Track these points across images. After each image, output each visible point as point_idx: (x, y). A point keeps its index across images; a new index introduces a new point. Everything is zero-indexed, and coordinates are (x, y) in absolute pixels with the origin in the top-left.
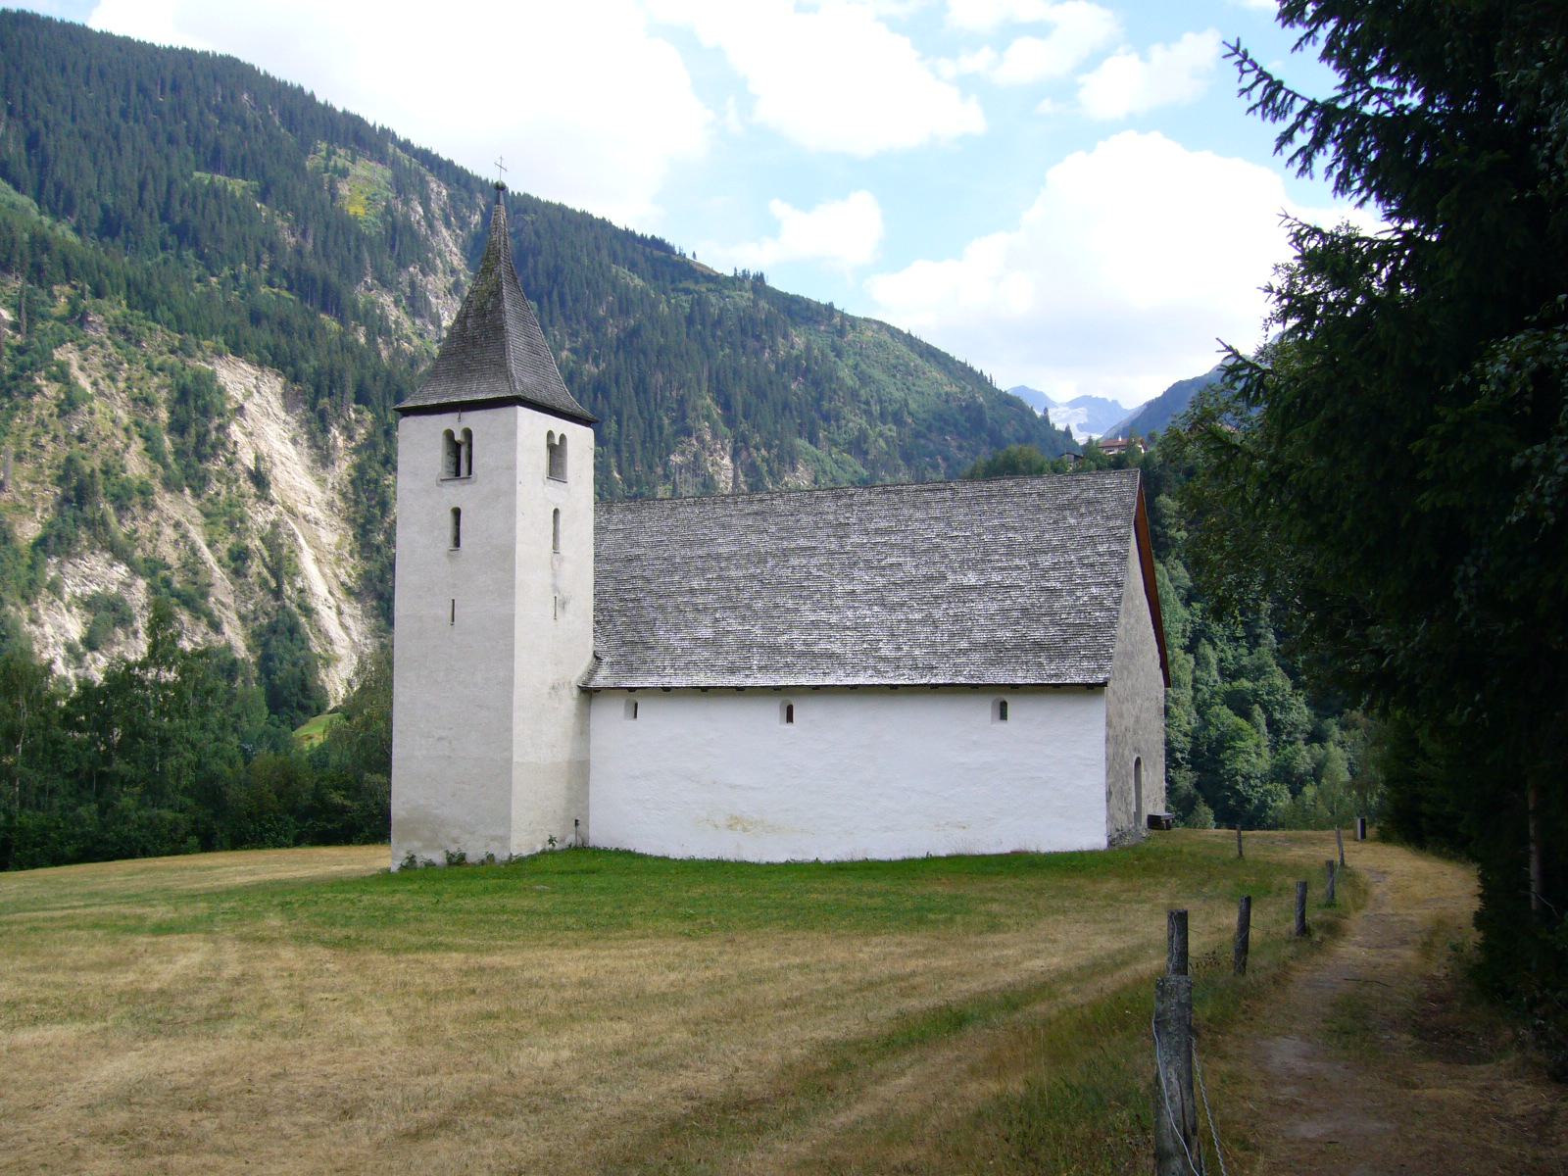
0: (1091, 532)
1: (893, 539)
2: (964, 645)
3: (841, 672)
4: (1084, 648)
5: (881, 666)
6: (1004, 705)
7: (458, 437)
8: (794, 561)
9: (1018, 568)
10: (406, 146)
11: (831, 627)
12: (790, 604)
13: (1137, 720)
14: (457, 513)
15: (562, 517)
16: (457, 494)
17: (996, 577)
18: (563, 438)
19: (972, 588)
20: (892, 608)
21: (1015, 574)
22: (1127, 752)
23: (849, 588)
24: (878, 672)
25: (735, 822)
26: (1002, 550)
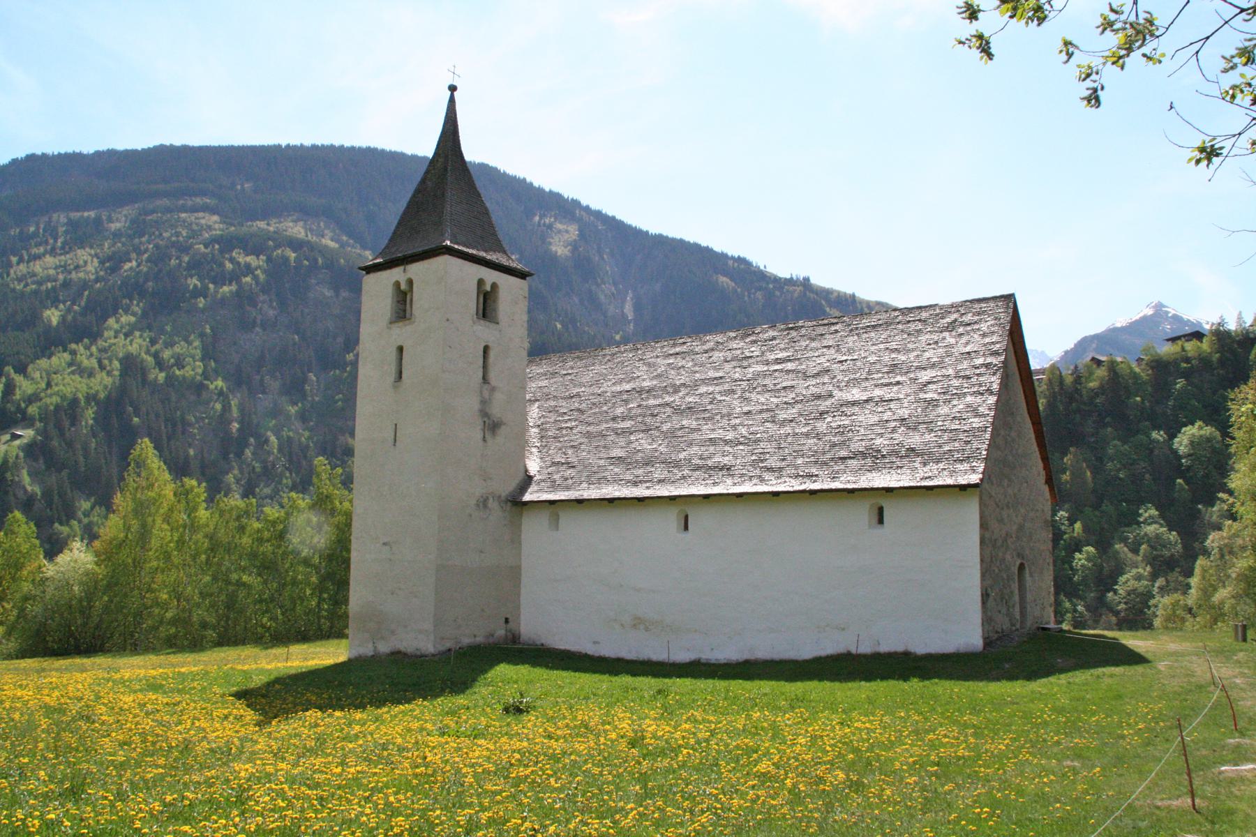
0: (968, 349)
1: (790, 366)
2: (843, 453)
3: (729, 481)
4: (958, 451)
5: (766, 476)
6: (881, 510)
7: (403, 287)
8: (703, 389)
9: (898, 383)
10: (587, 208)
11: (726, 442)
12: (694, 424)
13: (1021, 527)
14: (400, 349)
15: (492, 354)
16: (401, 334)
17: (878, 392)
18: (494, 286)
19: (854, 403)
20: (783, 423)
21: (895, 388)
22: (1008, 557)
23: (746, 409)
24: (762, 480)
25: (638, 623)
26: (885, 370)
